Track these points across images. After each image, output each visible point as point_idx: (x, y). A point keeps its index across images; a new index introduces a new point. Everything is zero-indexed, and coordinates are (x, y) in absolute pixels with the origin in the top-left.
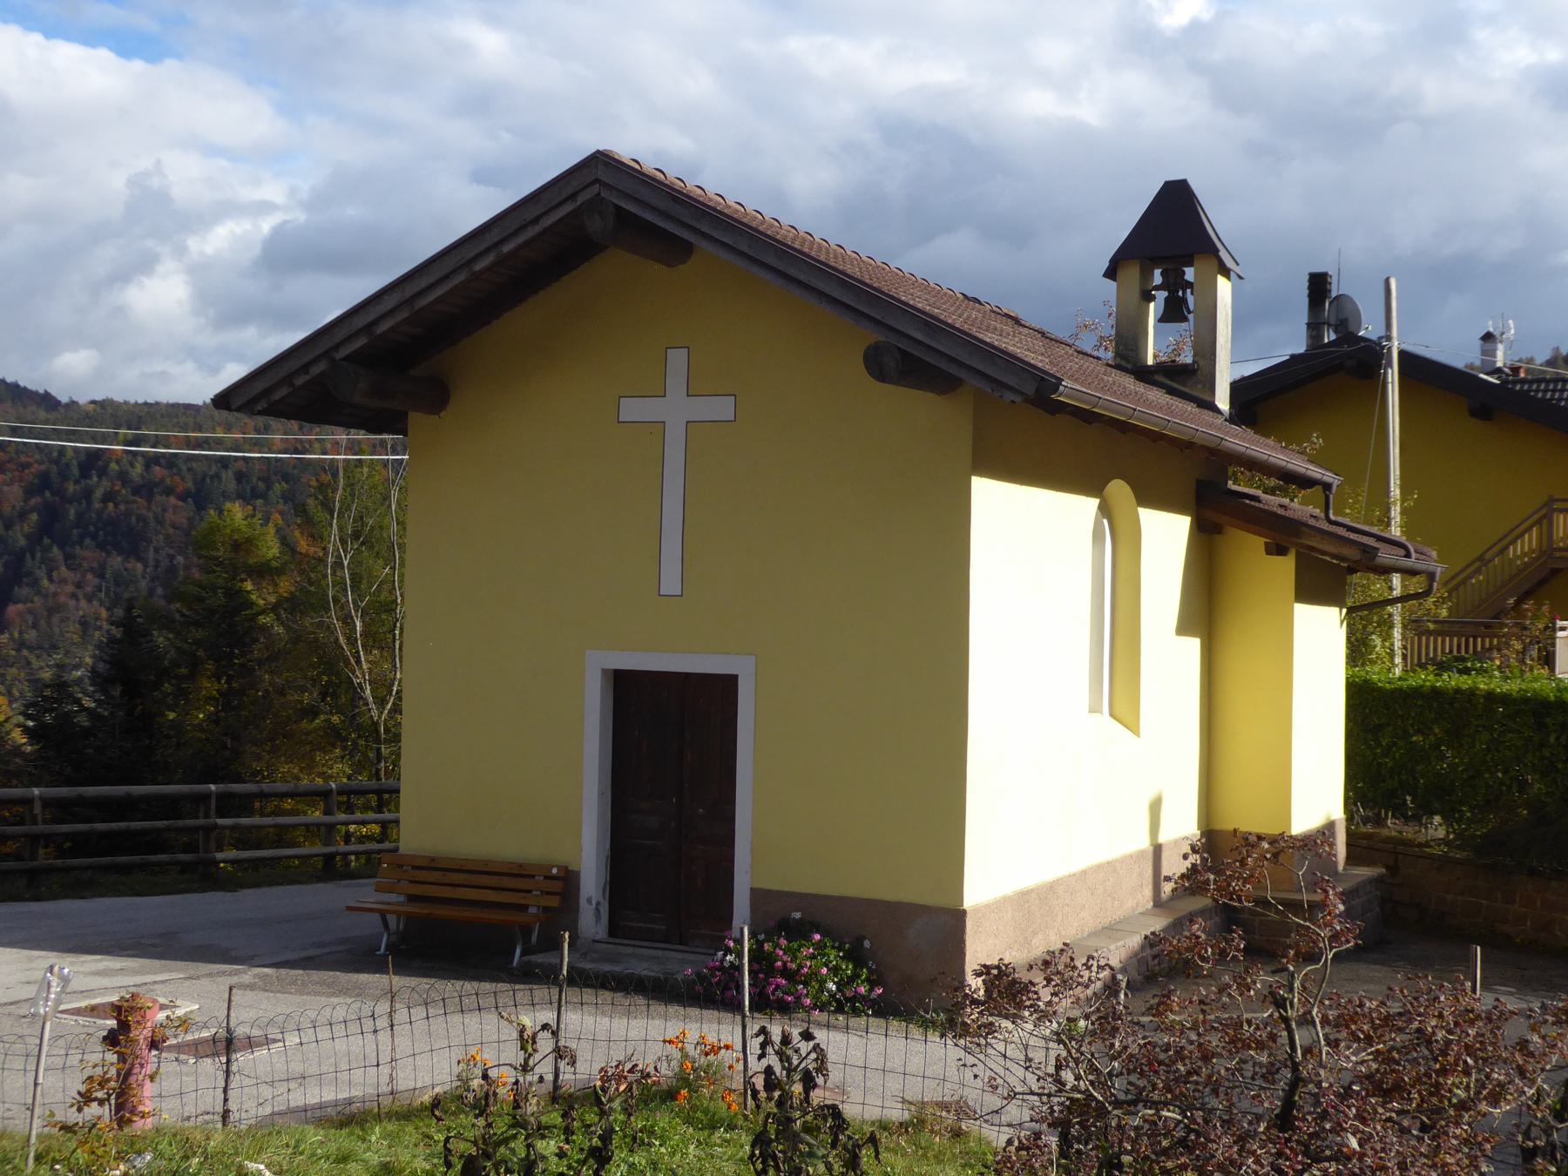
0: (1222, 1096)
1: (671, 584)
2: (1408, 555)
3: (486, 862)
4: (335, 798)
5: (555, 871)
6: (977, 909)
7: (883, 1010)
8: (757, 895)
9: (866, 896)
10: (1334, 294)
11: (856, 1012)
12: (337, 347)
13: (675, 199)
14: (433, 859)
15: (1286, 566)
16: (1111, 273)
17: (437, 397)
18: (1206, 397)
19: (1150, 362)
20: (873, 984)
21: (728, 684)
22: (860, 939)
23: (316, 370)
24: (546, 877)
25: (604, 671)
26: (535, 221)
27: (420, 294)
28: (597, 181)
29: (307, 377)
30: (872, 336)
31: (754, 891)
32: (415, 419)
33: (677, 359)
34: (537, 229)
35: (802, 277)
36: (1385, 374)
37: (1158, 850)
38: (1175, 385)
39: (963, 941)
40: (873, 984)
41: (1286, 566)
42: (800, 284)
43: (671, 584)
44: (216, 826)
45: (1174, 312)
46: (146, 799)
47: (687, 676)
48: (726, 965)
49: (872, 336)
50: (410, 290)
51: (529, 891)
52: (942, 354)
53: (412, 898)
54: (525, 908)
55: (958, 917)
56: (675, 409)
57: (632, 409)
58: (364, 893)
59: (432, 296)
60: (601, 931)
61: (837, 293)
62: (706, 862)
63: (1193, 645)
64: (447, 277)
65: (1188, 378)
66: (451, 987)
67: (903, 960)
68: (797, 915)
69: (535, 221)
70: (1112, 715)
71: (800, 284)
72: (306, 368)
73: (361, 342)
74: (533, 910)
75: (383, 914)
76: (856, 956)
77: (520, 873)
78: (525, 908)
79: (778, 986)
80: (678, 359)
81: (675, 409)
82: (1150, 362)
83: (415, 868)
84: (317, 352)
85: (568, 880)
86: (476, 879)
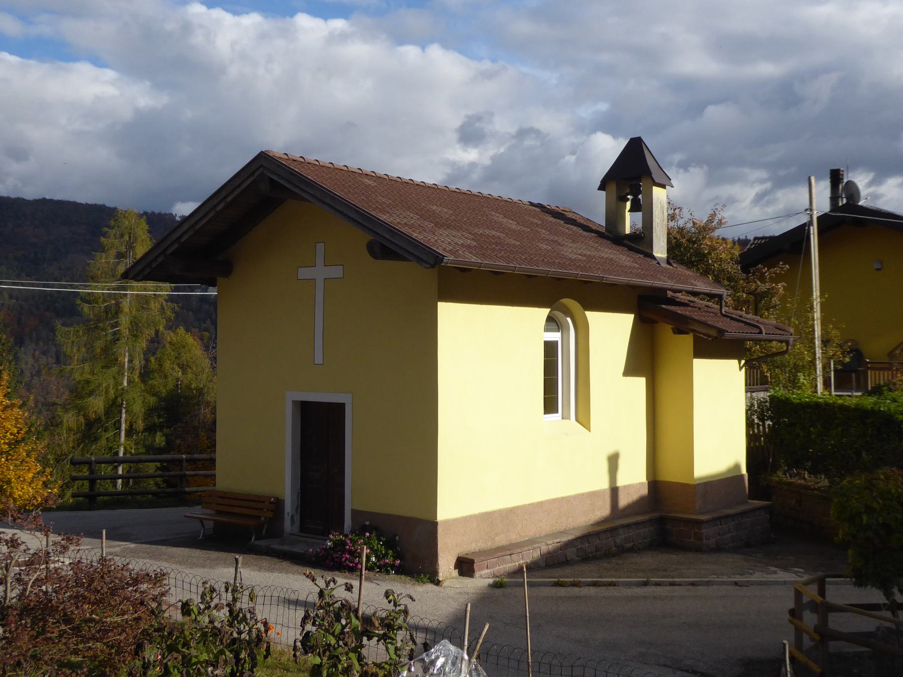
0: (397, 616)
1: (319, 359)
2: (761, 333)
4: (185, 464)
6: (447, 522)
8: (355, 513)
10: (845, 181)
11: (388, 572)
13: (291, 173)
15: (687, 341)
16: (602, 187)
17: (227, 269)
18: (649, 251)
19: (628, 231)
20: (395, 558)
22: (395, 536)
23: (160, 260)
25: (293, 402)
26: (239, 186)
27: (196, 223)
28: (262, 166)
30: (369, 237)
32: (220, 280)
33: (320, 247)
35: (341, 209)
36: (809, 230)
37: (614, 491)
38: (633, 245)
39: (436, 538)
40: (395, 558)
41: (687, 341)
42: (341, 213)
43: (319, 359)
44: (185, 475)
45: (635, 208)
47: (330, 404)
49: (369, 237)
52: (397, 245)
53: (219, 513)
55: (435, 524)
56: (319, 273)
57: (304, 273)
58: (197, 511)
59: (203, 222)
60: (296, 529)
61: (354, 216)
62: (346, 498)
63: (640, 383)
65: (640, 242)
66: (215, 554)
67: (409, 546)
69: (239, 186)
70: (577, 420)
71: (341, 213)
72: (155, 259)
73: (176, 246)
74: (263, 519)
75: (201, 520)
76: (390, 544)
79: (346, 559)
82: (628, 231)
85: (278, 504)
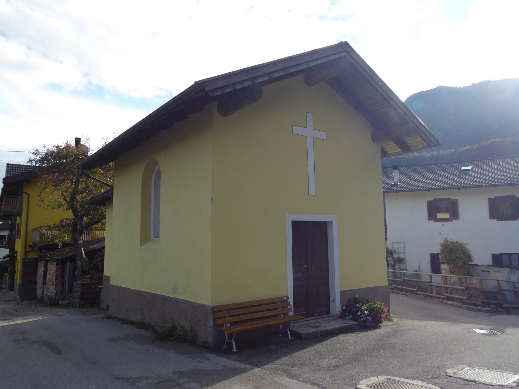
1: (312, 191)
3: (260, 301)
8: (342, 293)
12: (256, 77)
21: (296, 225)
23: (246, 84)
24: (281, 302)
33: (310, 116)
43: (312, 191)
46: (400, 288)
57: (297, 130)
72: (242, 82)
80: (310, 116)
81: (309, 133)
86: (269, 307)
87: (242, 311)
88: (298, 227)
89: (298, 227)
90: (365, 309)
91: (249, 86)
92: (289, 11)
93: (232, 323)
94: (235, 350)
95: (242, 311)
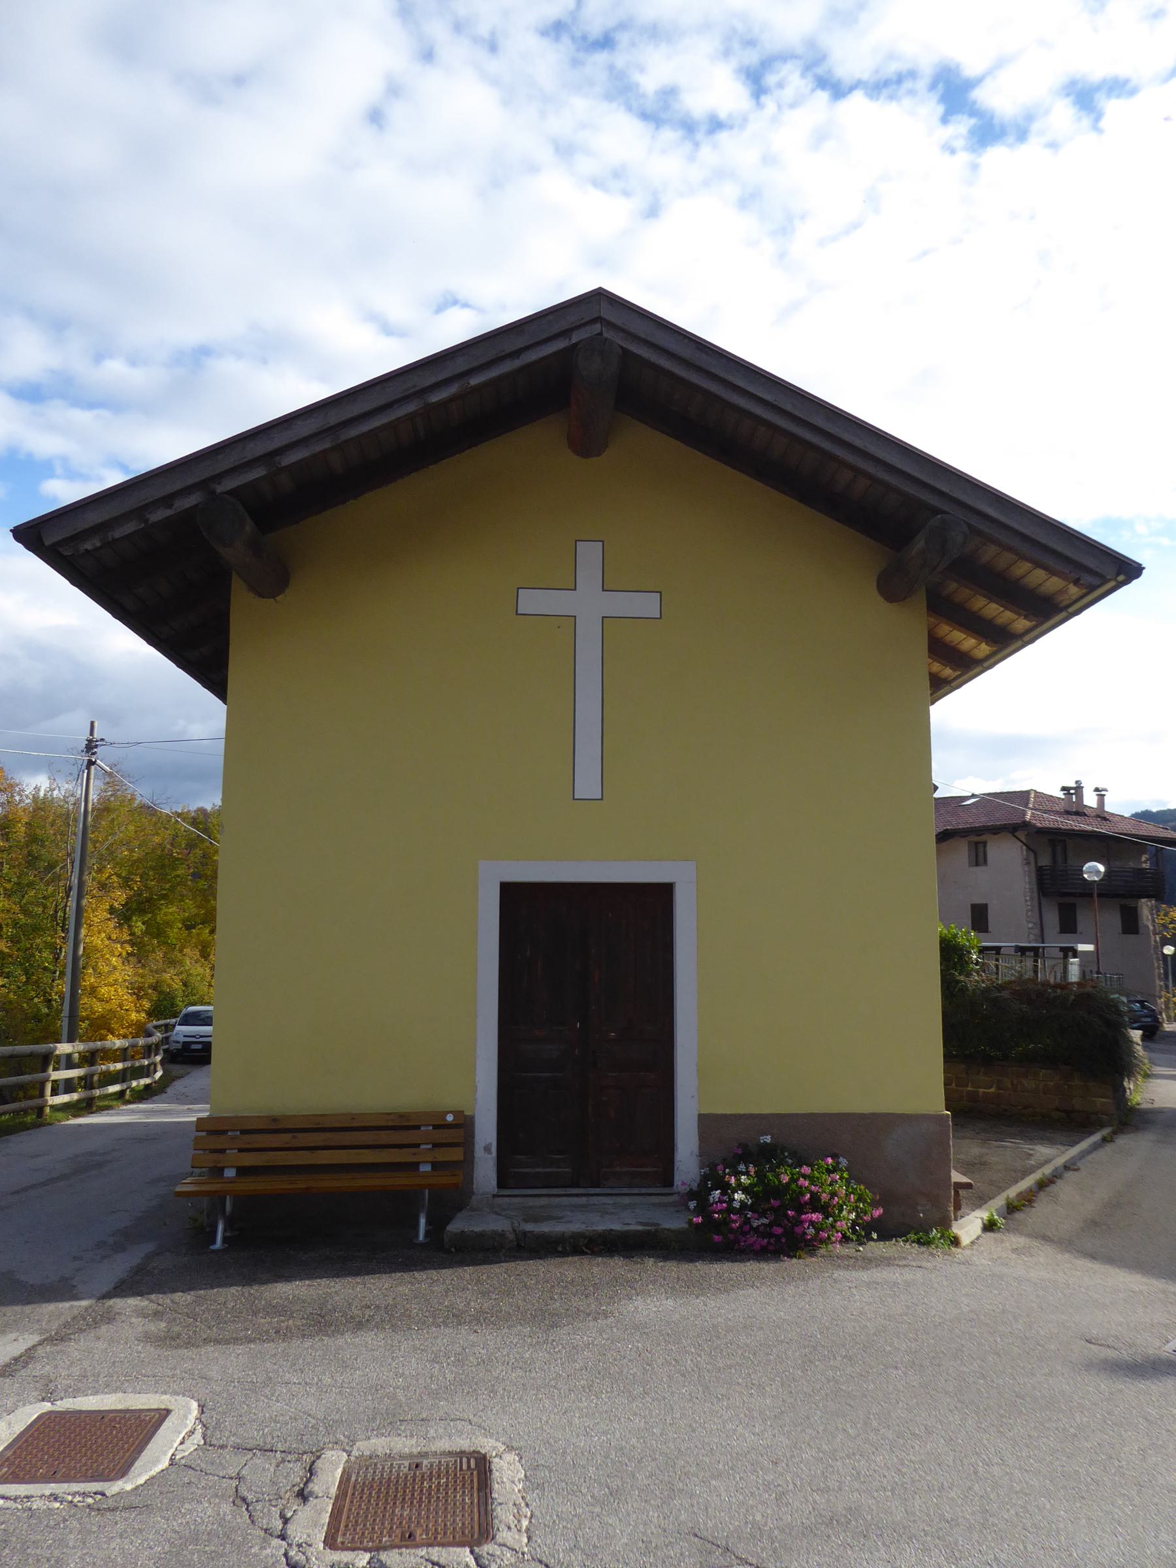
1: (588, 784)
3: (353, 1117)
5: (450, 1118)
7: (887, 1231)
8: (707, 1123)
9: (835, 1109)
12: (219, 477)
14: (275, 1120)
24: (436, 1127)
28: (599, 319)
29: (168, 512)
31: (702, 1118)
33: (589, 554)
34: (516, 364)
43: (588, 784)
48: (736, 1205)
50: (334, 418)
51: (418, 1146)
54: (415, 1166)
56: (588, 602)
57: (532, 601)
64: (389, 406)
68: (768, 1139)
72: (167, 500)
77: (402, 1125)
78: (415, 1166)
81: (588, 602)
83: (243, 1132)
84: (191, 481)
85: (465, 1124)
87: (285, 1139)
88: (974, 907)
89: (974, 907)
90: (740, 1187)
91: (196, 505)
92: (1166, 119)
93: (242, 1171)
94: (219, 1244)
95: (285, 1139)
